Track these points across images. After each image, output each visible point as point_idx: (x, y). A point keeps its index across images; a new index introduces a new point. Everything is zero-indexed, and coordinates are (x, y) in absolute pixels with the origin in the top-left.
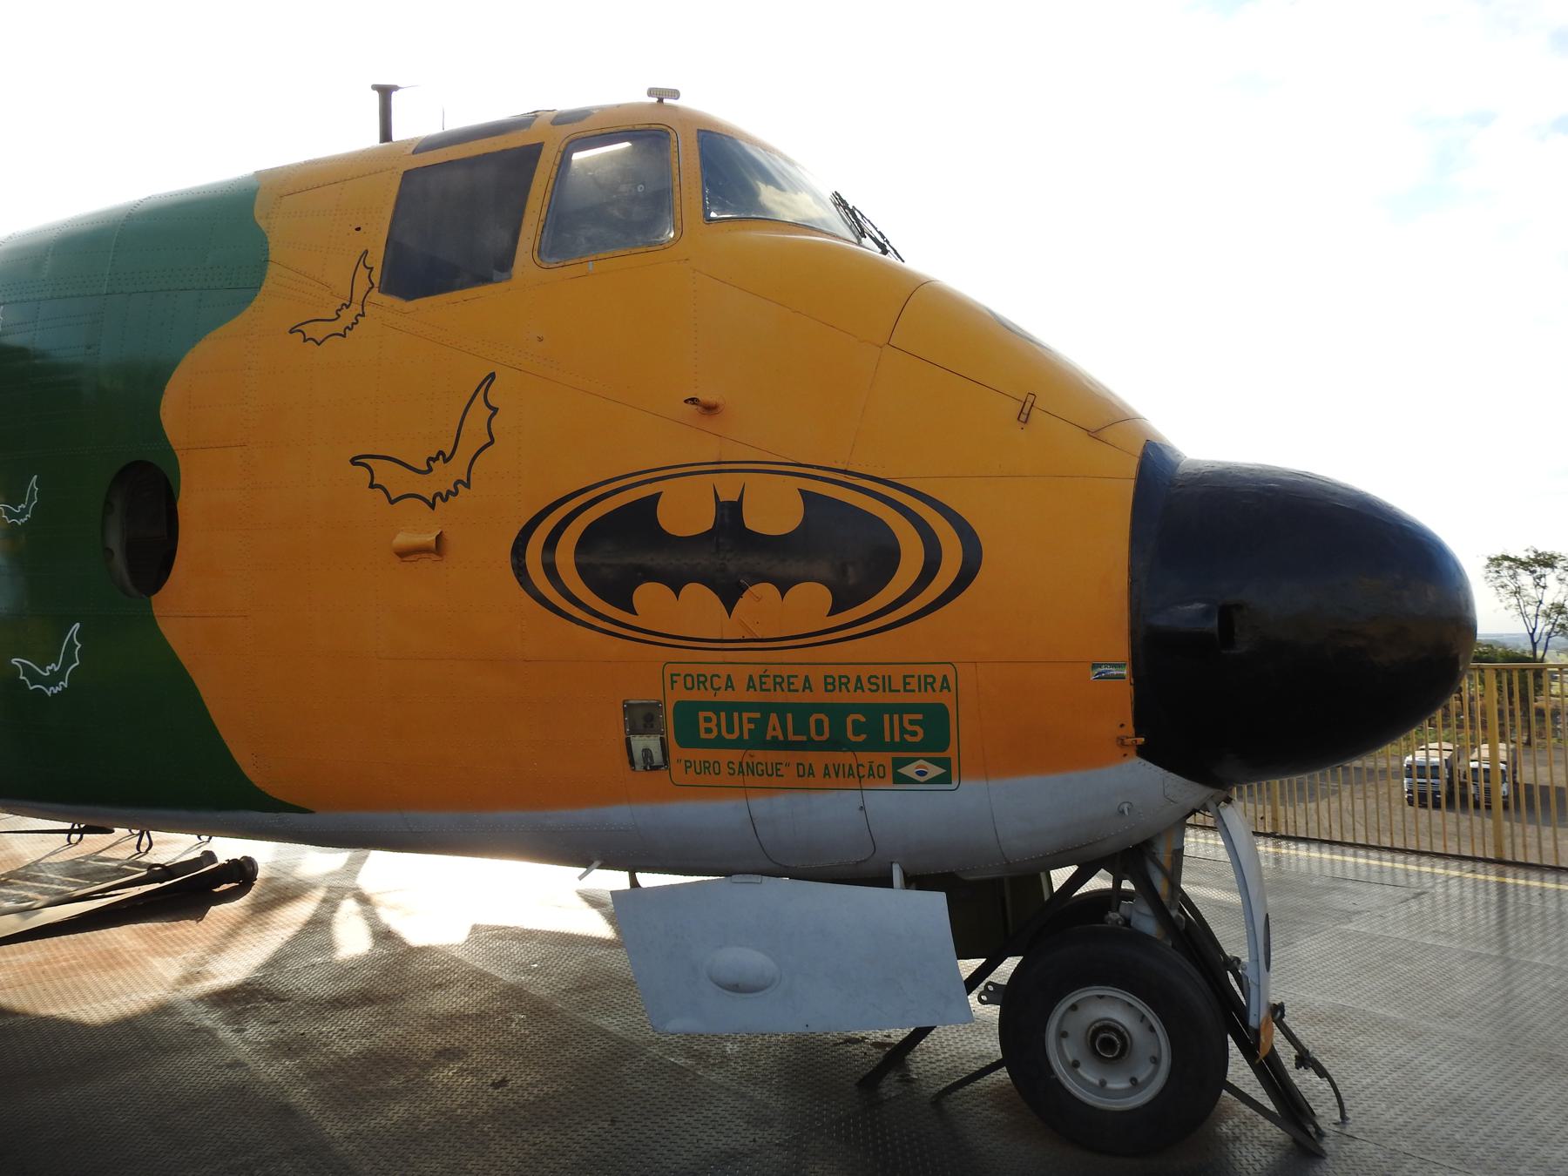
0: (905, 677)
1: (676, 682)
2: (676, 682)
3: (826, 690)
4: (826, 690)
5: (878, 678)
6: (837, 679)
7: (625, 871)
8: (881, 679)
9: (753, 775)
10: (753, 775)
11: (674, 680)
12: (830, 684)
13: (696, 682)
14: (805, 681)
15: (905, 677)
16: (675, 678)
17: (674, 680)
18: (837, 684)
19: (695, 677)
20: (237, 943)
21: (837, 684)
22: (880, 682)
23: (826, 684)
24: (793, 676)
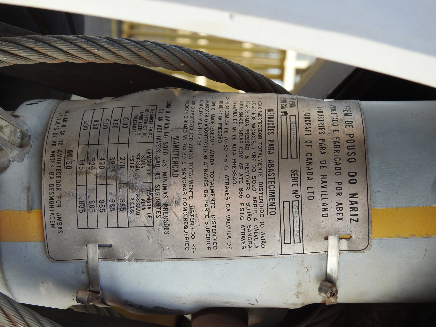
0: (186, 162)
1: (309, 147)
2: (309, 147)
3: (247, 203)
4: (247, 203)
5: (260, 188)
6: (248, 167)
7: (327, 305)
8: (159, 196)
9: (164, 134)
10: (164, 134)
11: (52, 189)
12: (255, 202)
13: (212, 122)
14: (339, 163)
15: (186, 162)
16: (206, 147)
17: (273, 200)
18: (255, 204)
19: (185, 229)
20: (220, 193)
21: (255, 204)
22: (261, 188)
23: (248, 203)
24: (188, 235)
